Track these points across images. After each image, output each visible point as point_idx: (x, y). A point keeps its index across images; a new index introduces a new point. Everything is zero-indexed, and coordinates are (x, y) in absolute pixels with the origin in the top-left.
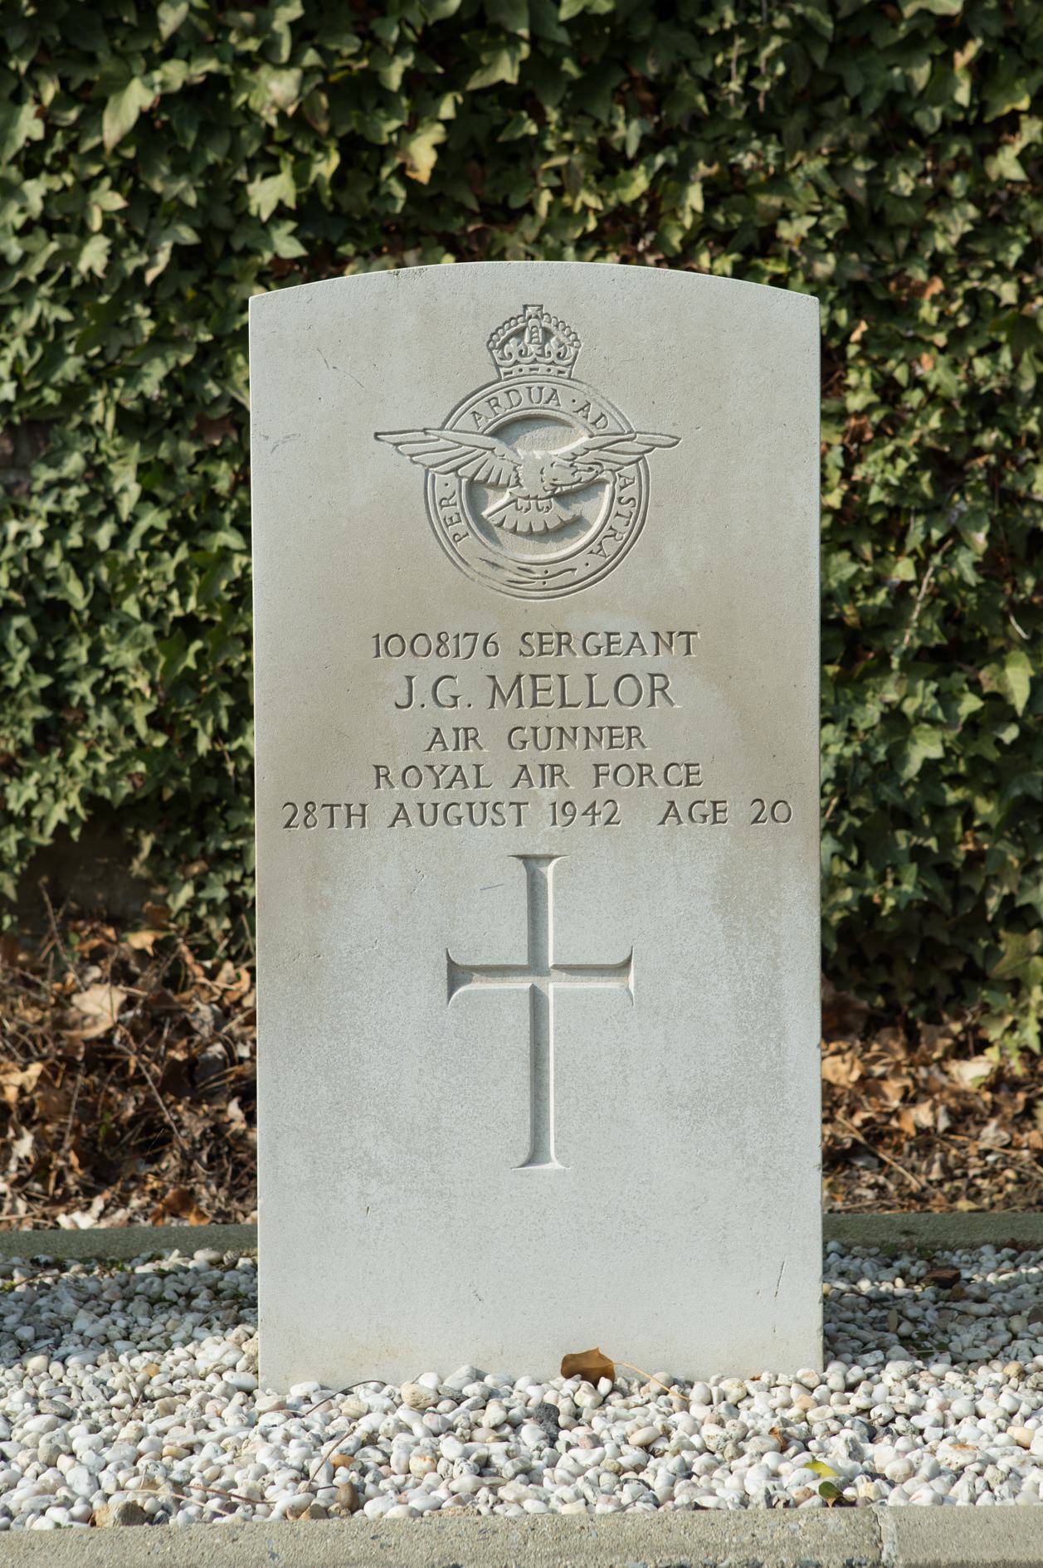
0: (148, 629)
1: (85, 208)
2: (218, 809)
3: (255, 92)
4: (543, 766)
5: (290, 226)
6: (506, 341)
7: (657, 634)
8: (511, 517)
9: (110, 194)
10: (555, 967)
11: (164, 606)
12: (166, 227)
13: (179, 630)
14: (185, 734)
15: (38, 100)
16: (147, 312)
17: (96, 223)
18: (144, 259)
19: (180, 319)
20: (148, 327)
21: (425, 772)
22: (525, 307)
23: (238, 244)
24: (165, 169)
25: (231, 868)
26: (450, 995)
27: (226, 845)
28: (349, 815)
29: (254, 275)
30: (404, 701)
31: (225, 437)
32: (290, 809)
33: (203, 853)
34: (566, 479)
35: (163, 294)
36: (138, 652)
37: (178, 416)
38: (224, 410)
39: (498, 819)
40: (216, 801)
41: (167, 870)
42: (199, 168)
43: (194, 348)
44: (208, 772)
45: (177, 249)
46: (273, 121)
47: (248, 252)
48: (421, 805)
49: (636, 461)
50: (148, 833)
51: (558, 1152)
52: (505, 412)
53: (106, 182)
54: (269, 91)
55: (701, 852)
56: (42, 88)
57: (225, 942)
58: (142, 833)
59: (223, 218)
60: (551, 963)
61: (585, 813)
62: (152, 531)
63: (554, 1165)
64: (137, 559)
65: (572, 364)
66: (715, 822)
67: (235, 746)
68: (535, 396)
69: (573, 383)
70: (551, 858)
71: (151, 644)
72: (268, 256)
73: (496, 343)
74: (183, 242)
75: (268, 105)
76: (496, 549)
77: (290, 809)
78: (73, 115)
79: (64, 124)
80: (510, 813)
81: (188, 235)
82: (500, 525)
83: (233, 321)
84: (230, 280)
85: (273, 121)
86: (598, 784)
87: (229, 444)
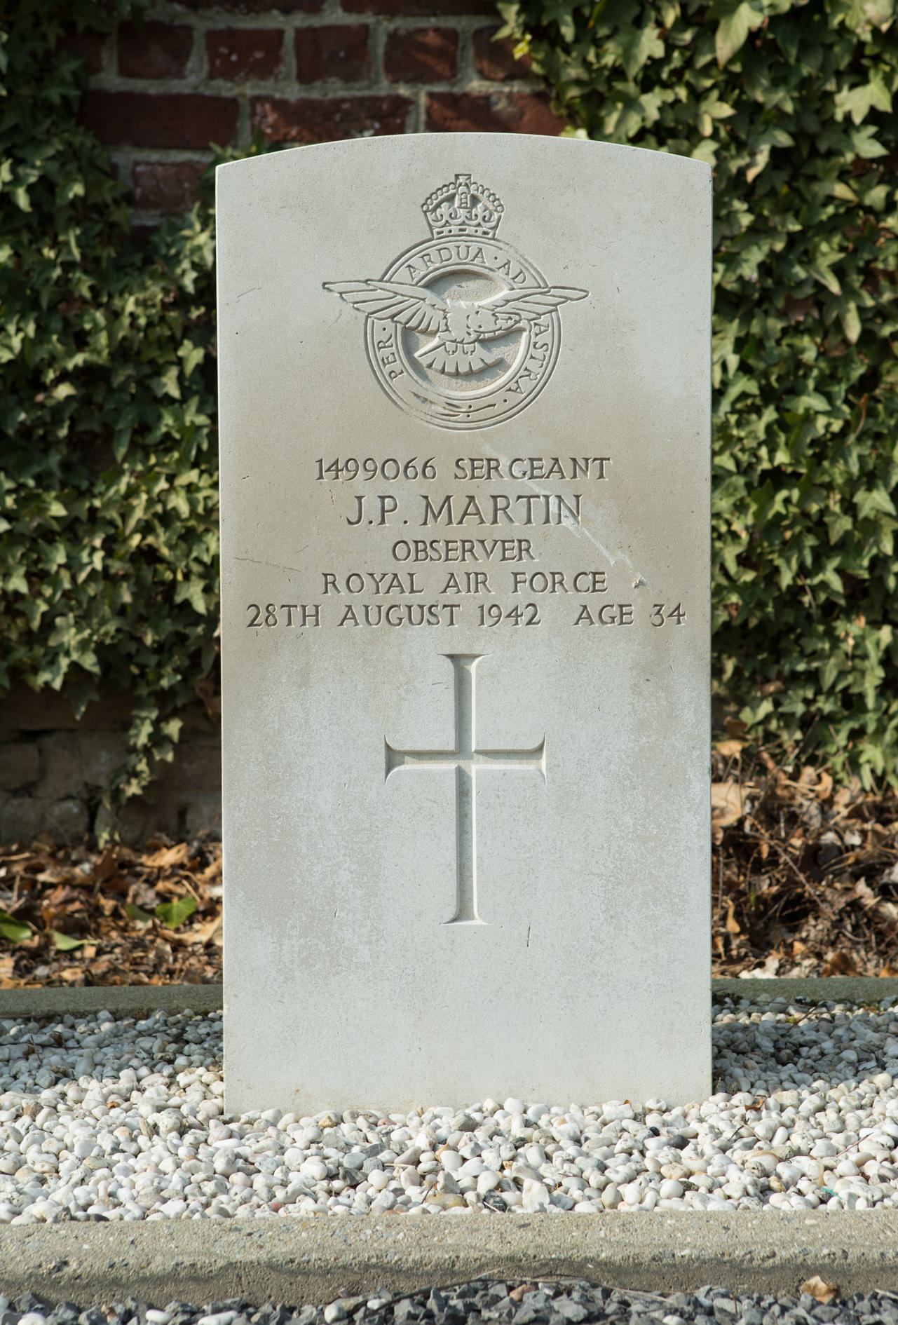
0: (740, 481)
1: (697, 116)
2: (792, 637)
3: (850, 12)
4: (468, 575)
5: (872, 130)
6: (438, 206)
7: (574, 460)
8: (440, 358)
9: (718, 104)
10: (478, 752)
11: (754, 460)
12: (764, 132)
13: (768, 481)
14: (768, 571)
15: (660, 24)
16: (745, 206)
17: (707, 129)
18: (747, 160)
19: (772, 212)
20: (746, 220)
21: (366, 579)
22: (457, 176)
23: (823, 147)
24: (765, 82)
25: (803, 687)
26: (388, 772)
27: (801, 667)
28: (305, 616)
29: (836, 174)
30: (354, 519)
31: (807, 314)
32: (253, 611)
33: (779, 676)
34: (490, 326)
35: (761, 191)
36: (732, 500)
37: (766, 296)
38: (809, 290)
39: (433, 620)
40: (791, 629)
41: (744, 689)
42: (794, 81)
43: (785, 237)
44: (785, 604)
45: (776, 152)
46: (867, 37)
47: (832, 153)
48: (367, 607)
49: (550, 312)
50: (730, 657)
52: (436, 265)
53: (715, 94)
54: (864, 12)
55: (617, 650)
56: (664, 13)
57: (797, 751)
58: (725, 656)
59: (812, 125)
61: (509, 616)
62: (744, 396)
63: (478, 921)
64: (727, 421)
65: (496, 227)
66: (622, 623)
67: (816, 580)
68: (463, 254)
69: (501, 245)
70: (476, 656)
71: (743, 493)
72: (849, 157)
73: (429, 207)
74: (779, 145)
75: (862, 23)
76: (425, 384)
77: (253, 611)
78: (688, 36)
79: (682, 44)
80: (444, 615)
81: (784, 139)
82: (430, 366)
83: (818, 214)
84: (814, 178)
85: (867, 37)
86: (516, 590)
87: (810, 320)
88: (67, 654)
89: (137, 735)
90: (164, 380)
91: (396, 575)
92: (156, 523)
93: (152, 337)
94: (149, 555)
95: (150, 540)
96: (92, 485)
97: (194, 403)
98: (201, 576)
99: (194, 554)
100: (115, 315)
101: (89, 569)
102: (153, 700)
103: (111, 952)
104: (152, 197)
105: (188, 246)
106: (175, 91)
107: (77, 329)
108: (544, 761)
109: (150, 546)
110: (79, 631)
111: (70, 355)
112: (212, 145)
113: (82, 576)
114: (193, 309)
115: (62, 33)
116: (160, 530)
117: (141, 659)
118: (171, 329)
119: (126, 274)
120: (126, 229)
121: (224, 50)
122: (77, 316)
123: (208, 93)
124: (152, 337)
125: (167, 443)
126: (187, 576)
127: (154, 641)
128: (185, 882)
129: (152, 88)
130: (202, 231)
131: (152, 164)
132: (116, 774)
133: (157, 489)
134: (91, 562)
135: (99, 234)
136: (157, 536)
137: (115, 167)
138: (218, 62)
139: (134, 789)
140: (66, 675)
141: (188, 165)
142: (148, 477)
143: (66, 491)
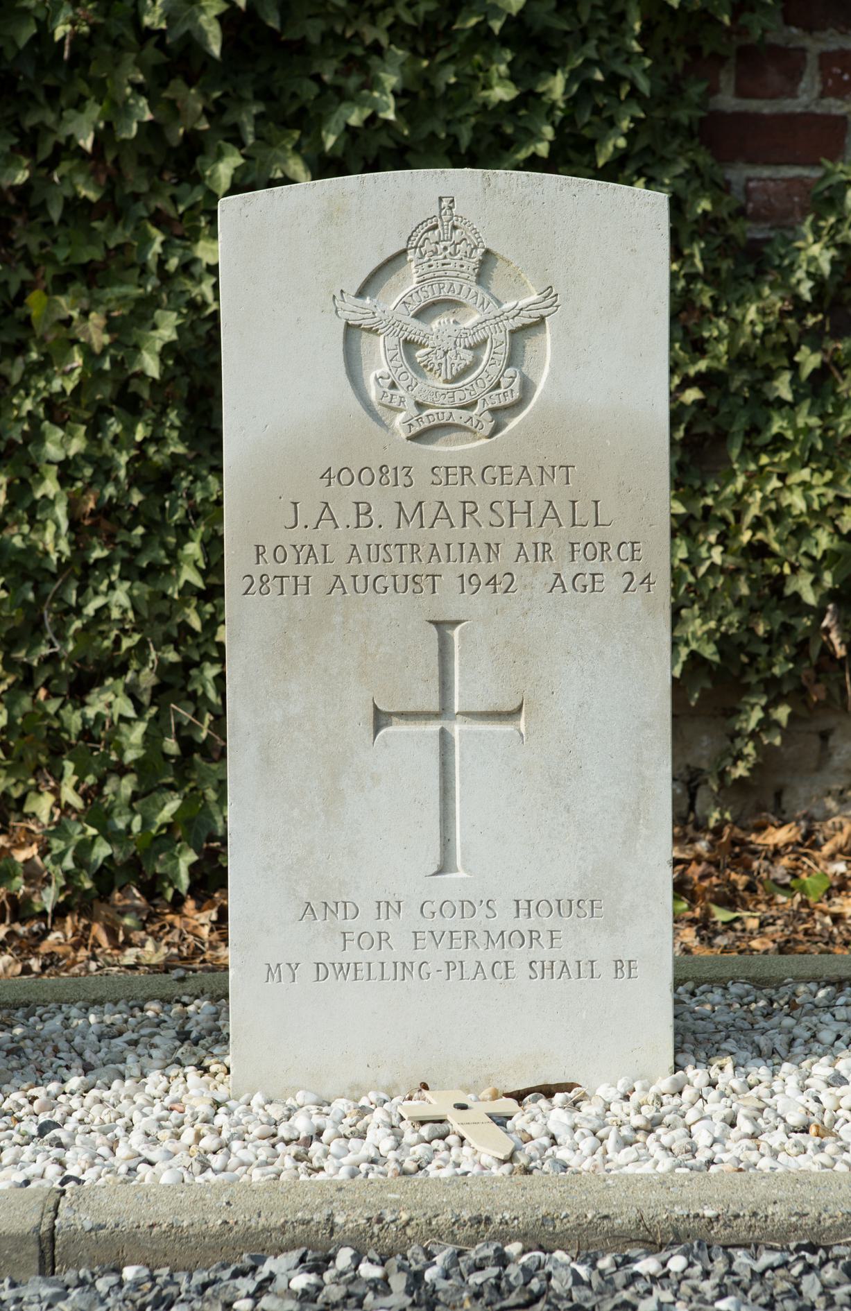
26: (376, 732)
39: (418, 589)
51: (464, 861)
60: (456, 710)
70: (458, 622)
88: (687, 643)
89: (747, 720)
90: (776, 384)
91: (312, 548)
92: (768, 520)
93: (769, 344)
94: (759, 551)
95: (760, 535)
96: (704, 484)
97: (805, 406)
98: (811, 570)
99: (803, 549)
100: (735, 324)
101: (708, 563)
102: (762, 687)
103: (773, 924)
104: (763, 211)
105: (803, 256)
106: (788, 110)
107: (696, 337)
108: (522, 722)
109: (760, 541)
110: (705, 622)
111: (694, 362)
112: (823, 160)
113: (702, 570)
114: (809, 316)
115: (687, 57)
116: (770, 526)
117: (753, 648)
118: (788, 335)
119: (741, 284)
120: (742, 242)
121: (837, 70)
122: (696, 324)
123: (819, 111)
124: (769, 344)
125: (779, 442)
126: (795, 569)
127: (766, 632)
128: (805, 859)
129: (766, 107)
130: (815, 242)
131: (764, 180)
132: (726, 753)
133: (769, 488)
134: (710, 557)
135: (718, 247)
136: (767, 532)
137: (728, 183)
138: (830, 82)
139: (741, 770)
140: (684, 663)
141: (799, 180)
142: (761, 475)
143: (681, 490)
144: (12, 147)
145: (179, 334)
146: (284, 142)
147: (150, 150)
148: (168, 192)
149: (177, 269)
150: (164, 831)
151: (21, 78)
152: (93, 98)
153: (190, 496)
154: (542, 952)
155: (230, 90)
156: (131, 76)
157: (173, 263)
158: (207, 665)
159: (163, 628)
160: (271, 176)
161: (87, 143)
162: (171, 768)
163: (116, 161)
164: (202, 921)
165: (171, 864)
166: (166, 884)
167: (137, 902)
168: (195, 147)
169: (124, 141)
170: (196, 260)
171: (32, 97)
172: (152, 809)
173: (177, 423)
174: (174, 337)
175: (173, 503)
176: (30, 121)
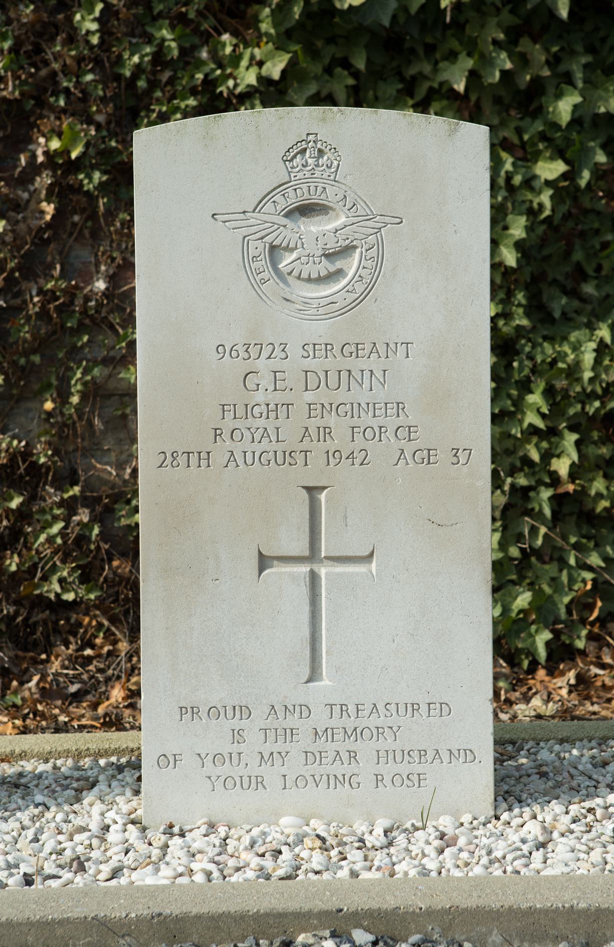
10: (325, 557)
63: (325, 682)
70: (324, 488)
108: (374, 564)
144: (398, 91)
145: (527, 233)
146: (607, 85)
147: (503, 93)
148: (513, 125)
149: (521, 183)
150: (521, 616)
151: (408, 37)
152: (464, 53)
153: (531, 358)
154: (388, 743)
155: (566, 46)
156: (494, 35)
157: (517, 180)
158: (543, 488)
159: (510, 460)
160: (596, 111)
161: (460, 87)
162: (513, 568)
163: (478, 101)
164: (559, 685)
165: (530, 641)
166: (523, 657)
167: (504, 670)
168: (537, 88)
169: (491, 85)
170: (535, 177)
171: (413, 51)
172: (509, 599)
173: (524, 302)
174: (524, 235)
175: (521, 363)
176: (412, 71)
